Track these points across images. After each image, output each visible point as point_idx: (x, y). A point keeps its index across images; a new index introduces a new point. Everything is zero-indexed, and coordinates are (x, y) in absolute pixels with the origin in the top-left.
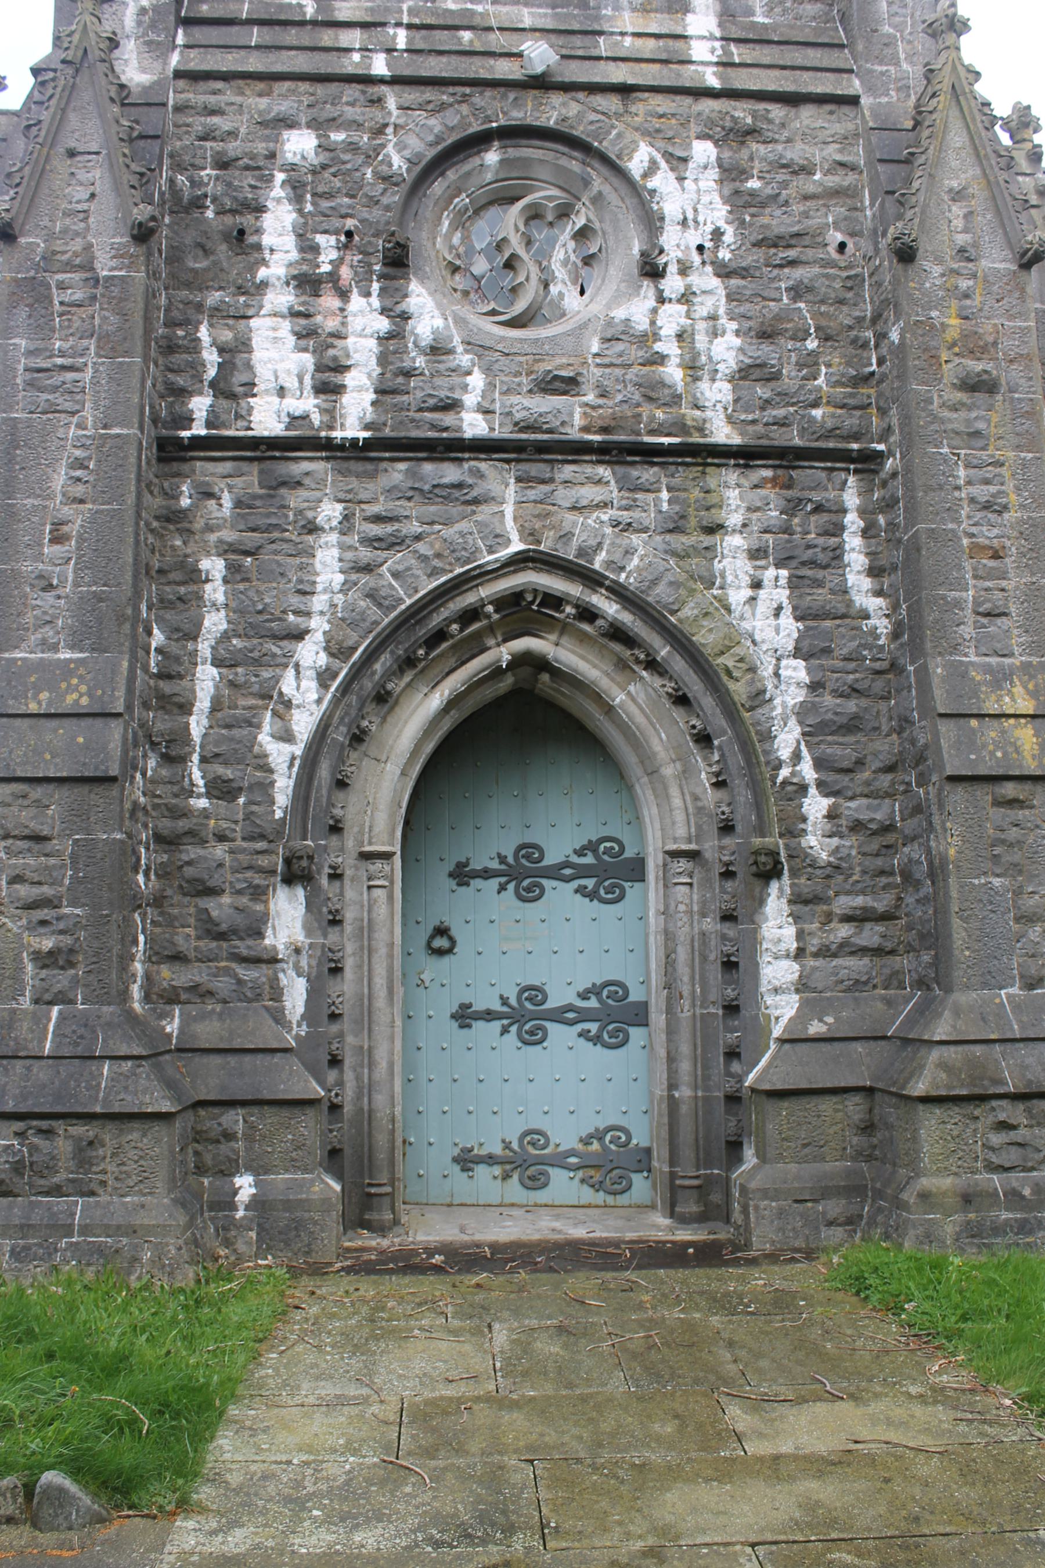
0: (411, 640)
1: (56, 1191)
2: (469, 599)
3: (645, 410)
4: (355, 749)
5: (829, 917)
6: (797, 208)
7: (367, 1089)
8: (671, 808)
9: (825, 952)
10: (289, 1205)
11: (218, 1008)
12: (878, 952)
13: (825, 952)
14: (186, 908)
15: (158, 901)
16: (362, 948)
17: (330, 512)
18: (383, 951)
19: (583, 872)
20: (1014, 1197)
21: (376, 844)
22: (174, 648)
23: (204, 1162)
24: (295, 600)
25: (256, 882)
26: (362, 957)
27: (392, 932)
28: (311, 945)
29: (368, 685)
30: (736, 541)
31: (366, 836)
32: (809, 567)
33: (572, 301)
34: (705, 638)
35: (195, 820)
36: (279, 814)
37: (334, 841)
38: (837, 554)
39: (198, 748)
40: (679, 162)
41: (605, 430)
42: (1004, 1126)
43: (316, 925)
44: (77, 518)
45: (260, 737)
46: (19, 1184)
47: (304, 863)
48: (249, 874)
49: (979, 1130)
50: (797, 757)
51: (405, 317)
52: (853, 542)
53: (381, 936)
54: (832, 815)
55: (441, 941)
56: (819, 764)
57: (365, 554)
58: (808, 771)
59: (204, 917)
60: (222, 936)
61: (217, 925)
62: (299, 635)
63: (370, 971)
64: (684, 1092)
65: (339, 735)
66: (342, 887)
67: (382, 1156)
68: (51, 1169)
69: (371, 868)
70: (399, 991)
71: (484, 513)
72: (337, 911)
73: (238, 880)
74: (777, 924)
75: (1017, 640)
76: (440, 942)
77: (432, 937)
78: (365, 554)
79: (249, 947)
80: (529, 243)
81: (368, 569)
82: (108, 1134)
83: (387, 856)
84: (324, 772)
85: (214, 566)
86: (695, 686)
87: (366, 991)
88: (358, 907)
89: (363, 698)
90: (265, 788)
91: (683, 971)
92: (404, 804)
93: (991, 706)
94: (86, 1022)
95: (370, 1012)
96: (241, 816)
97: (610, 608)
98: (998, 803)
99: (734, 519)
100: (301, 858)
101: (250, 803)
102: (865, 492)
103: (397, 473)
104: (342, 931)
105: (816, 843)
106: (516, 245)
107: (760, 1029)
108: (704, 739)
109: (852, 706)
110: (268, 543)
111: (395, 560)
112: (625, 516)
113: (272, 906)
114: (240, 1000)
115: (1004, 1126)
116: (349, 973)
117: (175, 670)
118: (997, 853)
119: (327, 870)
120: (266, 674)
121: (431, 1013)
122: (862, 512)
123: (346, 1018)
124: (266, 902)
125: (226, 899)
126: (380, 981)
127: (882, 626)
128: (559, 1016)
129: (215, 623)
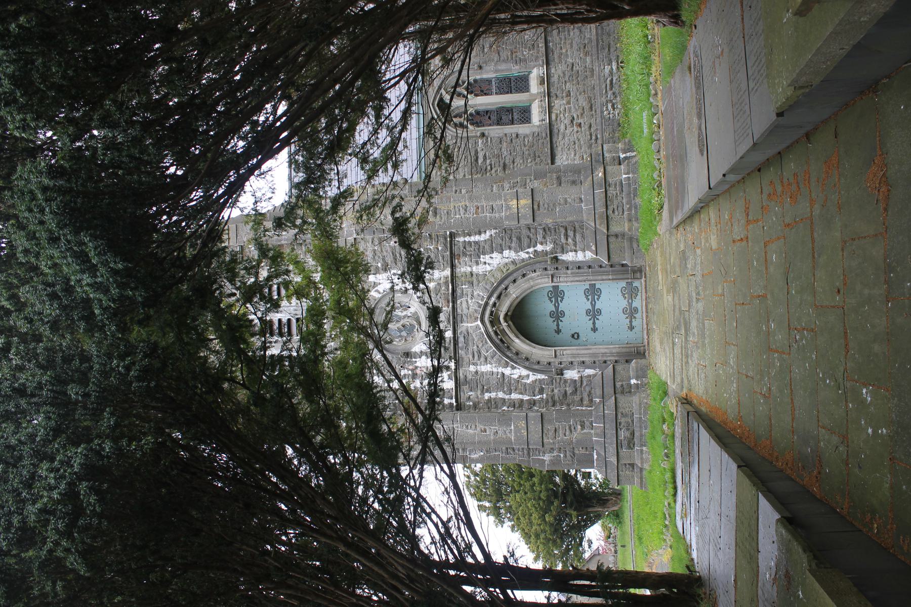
0: (502, 346)
1: (633, 421)
2: (492, 334)
3: (442, 292)
5: (567, 244)
6: (385, 254)
7: (612, 354)
8: (541, 282)
9: (575, 245)
10: (637, 371)
12: (575, 231)
13: (575, 245)
14: (570, 398)
15: (568, 405)
17: (472, 368)
19: (557, 301)
20: (630, 209)
22: (507, 404)
23: (628, 390)
24: (495, 376)
29: (514, 357)
30: (474, 268)
32: (479, 250)
33: (412, 310)
34: (499, 276)
38: (476, 243)
40: (375, 284)
41: (448, 302)
42: (613, 212)
44: (481, 427)
46: (631, 429)
49: (615, 217)
50: (528, 253)
51: (421, 352)
52: (472, 239)
53: (575, 352)
54: (542, 244)
55: (575, 336)
56: (529, 247)
57: (482, 359)
58: (531, 250)
62: (503, 374)
64: (610, 277)
65: (527, 364)
67: (628, 350)
68: (628, 422)
70: (589, 347)
71: (471, 331)
74: (569, 257)
75: (499, 203)
76: (576, 336)
78: (482, 359)
80: (398, 321)
81: (486, 359)
82: (620, 410)
83: (555, 351)
84: (536, 367)
85: (487, 396)
86: (511, 278)
89: (517, 358)
91: (581, 278)
93: (516, 210)
94: (596, 417)
97: (493, 299)
98: (539, 209)
99: (469, 269)
102: (459, 235)
103: (461, 352)
105: (549, 247)
106: (399, 325)
107: (594, 260)
108: (524, 275)
109: (514, 239)
110: (481, 383)
111: (483, 352)
112: (469, 296)
115: (613, 212)
117: (513, 404)
118: (551, 209)
122: (465, 236)
126: (586, 352)
127: (493, 231)
128: (593, 306)
129: (501, 395)
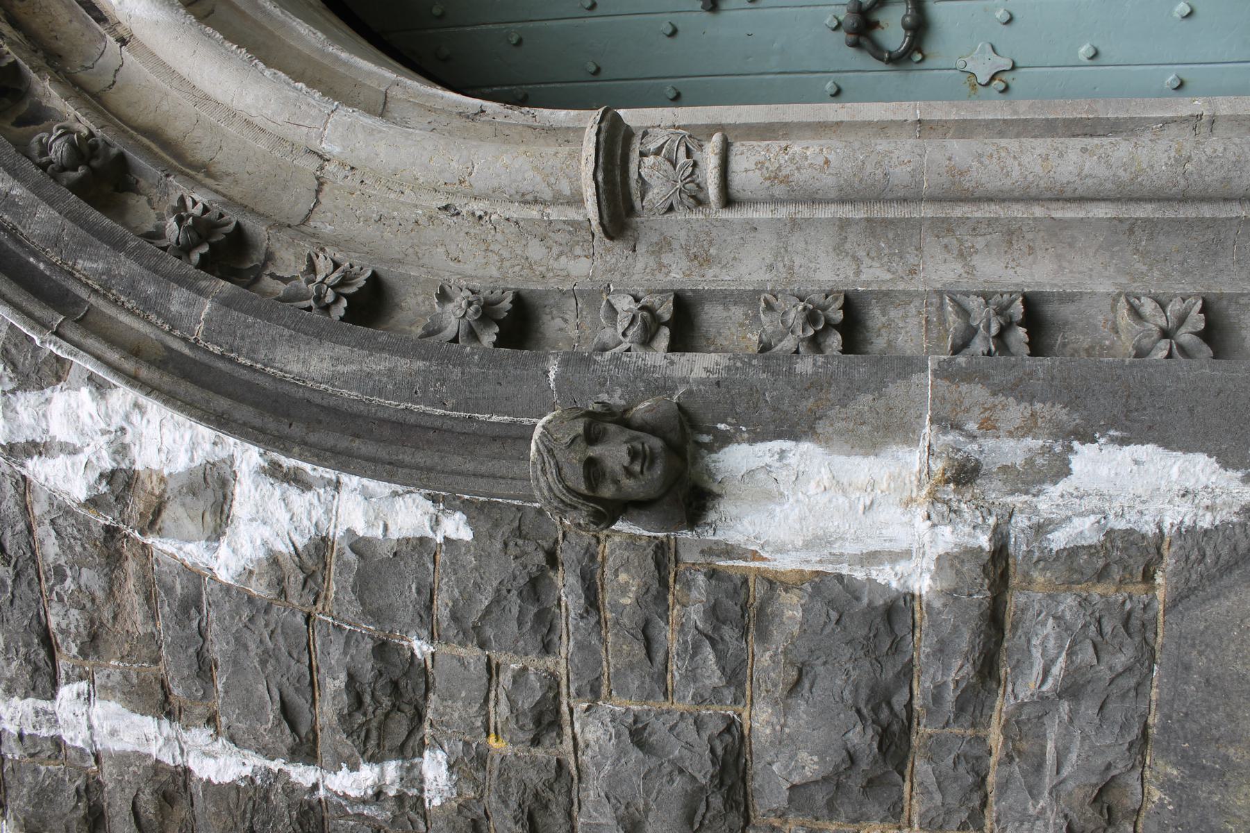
4: (269, 257)
11: (1162, 767)
16: (944, 227)
18: (959, 150)
21: (575, 179)
25: (696, 615)
26: (975, 228)
27: (882, 128)
28: (947, 423)
31: (554, 213)
35: (492, 801)
36: (456, 527)
37: (562, 326)
39: (276, 765)
43: (865, 401)
45: (224, 576)
47: (614, 453)
48: (669, 638)
53: (901, 158)
59: (820, 798)
60: (894, 743)
61: (852, 758)
63: (1027, 198)
66: (726, 298)
69: (658, 192)
72: (811, 317)
73: (692, 675)
77: (877, 51)
79: (942, 650)
83: (615, 147)
84: (315, 363)
87: (1101, 211)
88: (797, 241)
90: (374, 565)
92: (474, 103)
95: (1184, 199)
96: (472, 653)
100: (593, 468)
101: (425, 616)
104: (886, 297)
113: (785, 563)
114: (1140, 689)
116: (1038, 273)
119: (658, 356)
120: (51, 549)
121: (1084, 51)
123: (1222, 286)
124: (773, 582)
125: (761, 720)
